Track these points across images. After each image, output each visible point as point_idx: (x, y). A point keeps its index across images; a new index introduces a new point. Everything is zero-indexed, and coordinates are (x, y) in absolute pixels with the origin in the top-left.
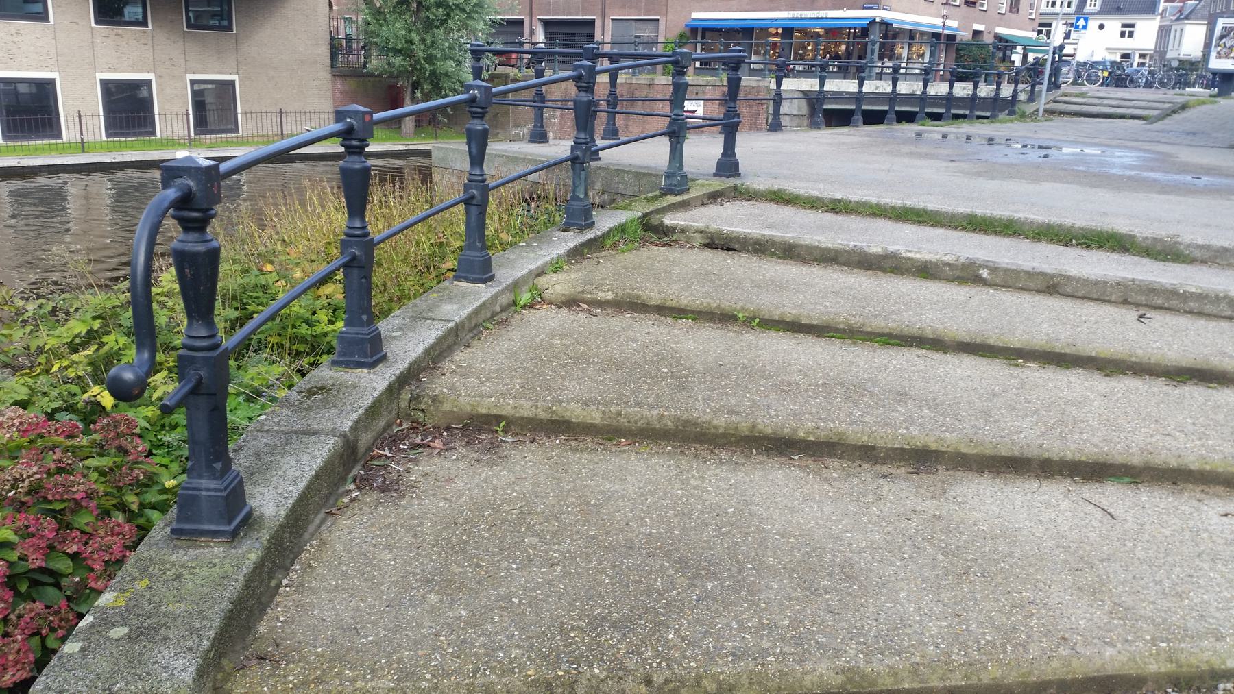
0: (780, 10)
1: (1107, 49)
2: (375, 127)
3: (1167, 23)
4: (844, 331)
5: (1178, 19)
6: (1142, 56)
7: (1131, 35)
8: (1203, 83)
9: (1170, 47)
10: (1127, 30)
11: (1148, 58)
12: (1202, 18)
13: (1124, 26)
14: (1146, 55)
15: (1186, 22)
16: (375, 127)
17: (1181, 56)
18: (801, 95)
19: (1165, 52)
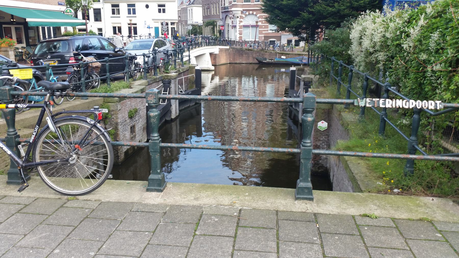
0: (44, 3)
1: (153, 20)
2: (202, 72)
3: (185, 6)
4: (388, 158)
5: (189, 4)
6: (172, 24)
7: (164, 11)
8: (206, 42)
9: (188, 19)
10: (162, 8)
11: (176, 24)
12: (200, 4)
13: (159, 6)
14: (175, 22)
15: (193, 5)
16: (202, 72)
17: (194, 23)
18: (256, 61)
19: (187, 21)
